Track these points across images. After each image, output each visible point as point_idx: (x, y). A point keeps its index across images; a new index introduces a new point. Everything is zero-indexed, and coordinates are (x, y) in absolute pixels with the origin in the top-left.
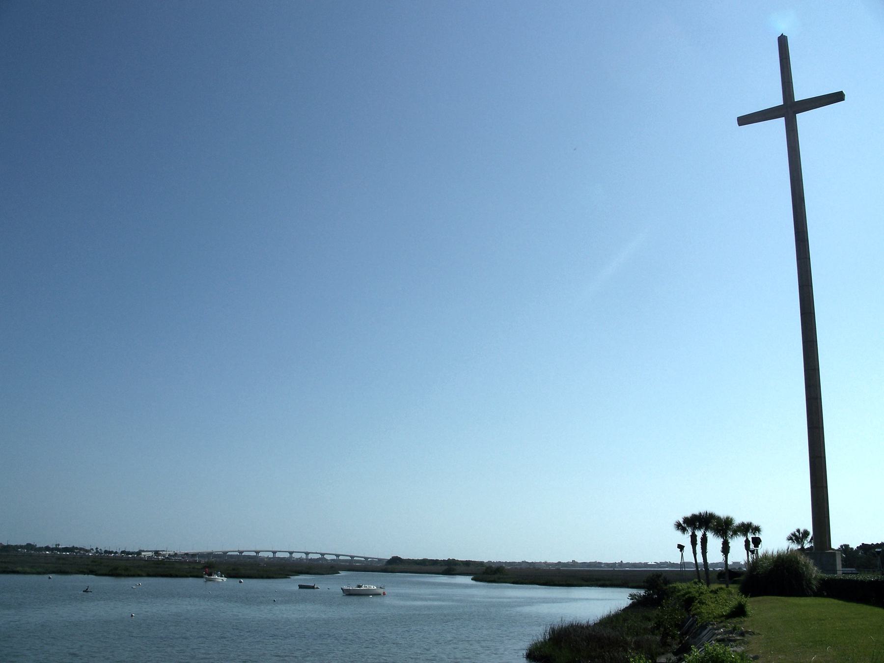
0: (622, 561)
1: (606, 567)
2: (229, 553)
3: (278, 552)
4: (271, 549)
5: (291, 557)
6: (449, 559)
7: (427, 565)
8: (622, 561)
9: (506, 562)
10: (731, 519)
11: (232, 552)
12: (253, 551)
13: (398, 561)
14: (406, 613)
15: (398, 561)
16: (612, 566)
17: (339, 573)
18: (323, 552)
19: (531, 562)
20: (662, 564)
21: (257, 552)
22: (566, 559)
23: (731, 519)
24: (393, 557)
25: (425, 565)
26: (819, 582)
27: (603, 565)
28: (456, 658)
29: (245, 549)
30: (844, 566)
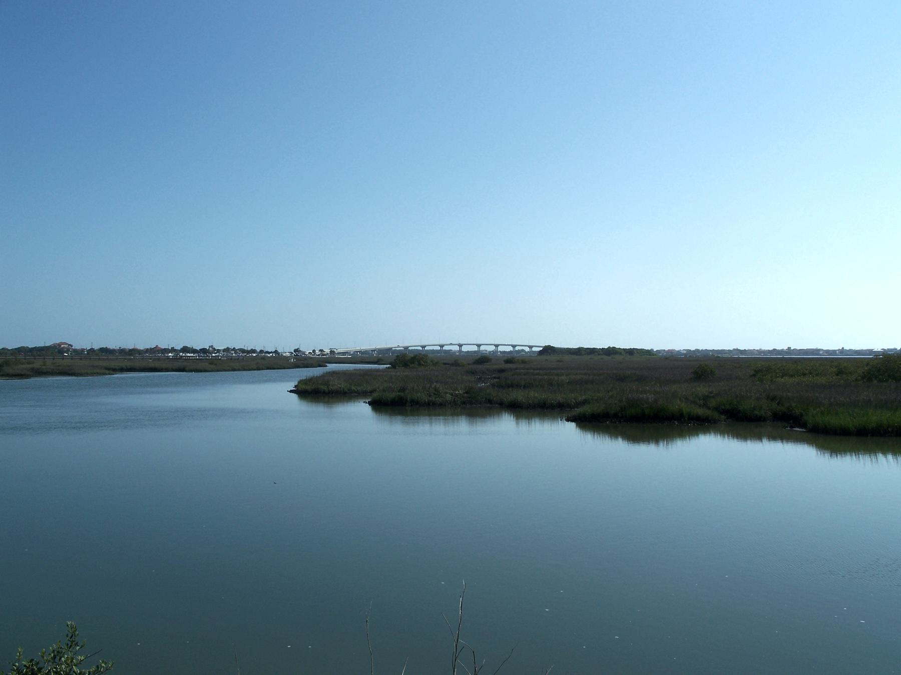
0: (843, 348)
1: (839, 354)
2: (410, 348)
3: (482, 346)
5: (460, 351)
6: (609, 347)
8: (843, 348)
9: (713, 350)
10: (734, 438)
11: (417, 346)
12: (437, 345)
13: (549, 351)
16: (831, 354)
17: (326, 366)
18: (496, 343)
19: (743, 349)
20: (889, 351)
21: (442, 346)
22: (782, 346)
23: (734, 438)
25: (581, 354)
27: (821, 352)
29: (409, 345)
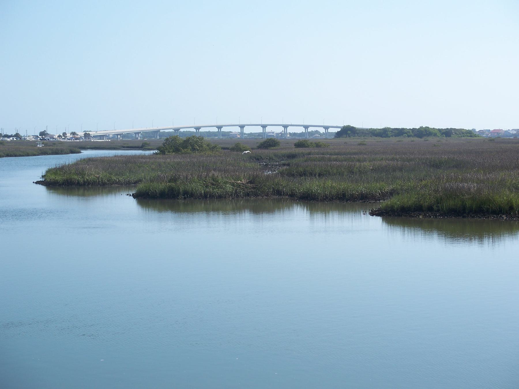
0: (422, 126)
2: (182, 130)
4: (238, 123)
5: (242, 133)
6: (421, 127)
7: (389, 137)
13: (349, 132)
14: (114, 178)
15: (349, 132)
21: (220, 127)
24: (348, 125)
25: (387, 136)
26: (500, 237)
28: (503, 236)
30: (140, 138)
